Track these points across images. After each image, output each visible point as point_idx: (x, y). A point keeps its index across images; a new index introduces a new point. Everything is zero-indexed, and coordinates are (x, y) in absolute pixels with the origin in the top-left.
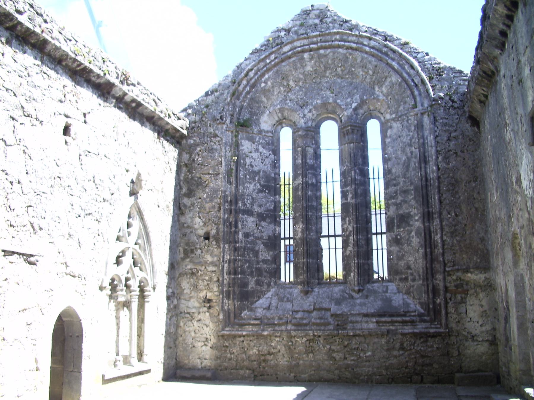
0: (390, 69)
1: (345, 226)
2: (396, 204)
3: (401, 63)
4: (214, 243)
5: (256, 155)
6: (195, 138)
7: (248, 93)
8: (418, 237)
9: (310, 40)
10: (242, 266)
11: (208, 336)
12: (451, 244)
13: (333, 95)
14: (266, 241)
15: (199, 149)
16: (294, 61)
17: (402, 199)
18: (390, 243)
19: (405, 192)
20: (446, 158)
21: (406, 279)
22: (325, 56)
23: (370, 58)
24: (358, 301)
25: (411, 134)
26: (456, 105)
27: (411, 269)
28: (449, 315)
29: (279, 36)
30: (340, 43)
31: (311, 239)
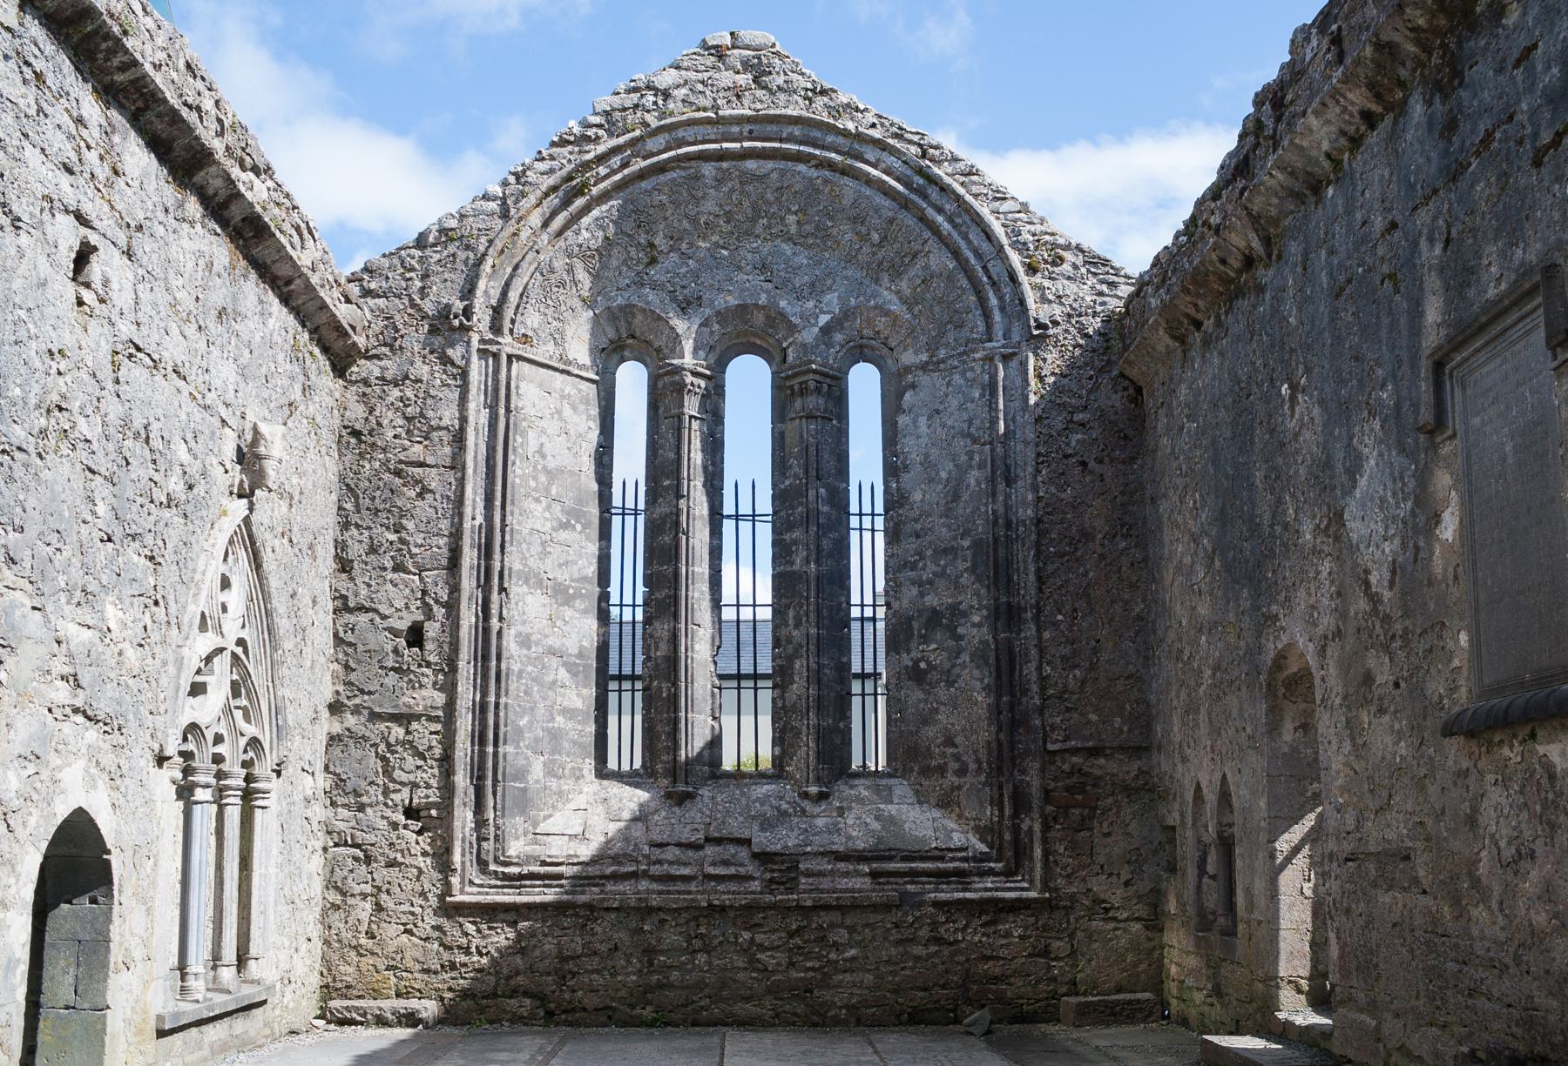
0: (927, 234)
3: (959, 220)
13: (770, 285)
16: (674, 180)
17: (938, 569)
19: (950, 551)
22: (761, 178)
23: (879, 199)
24: (820, 822)
27: (955, 746)
30: (802, 148)
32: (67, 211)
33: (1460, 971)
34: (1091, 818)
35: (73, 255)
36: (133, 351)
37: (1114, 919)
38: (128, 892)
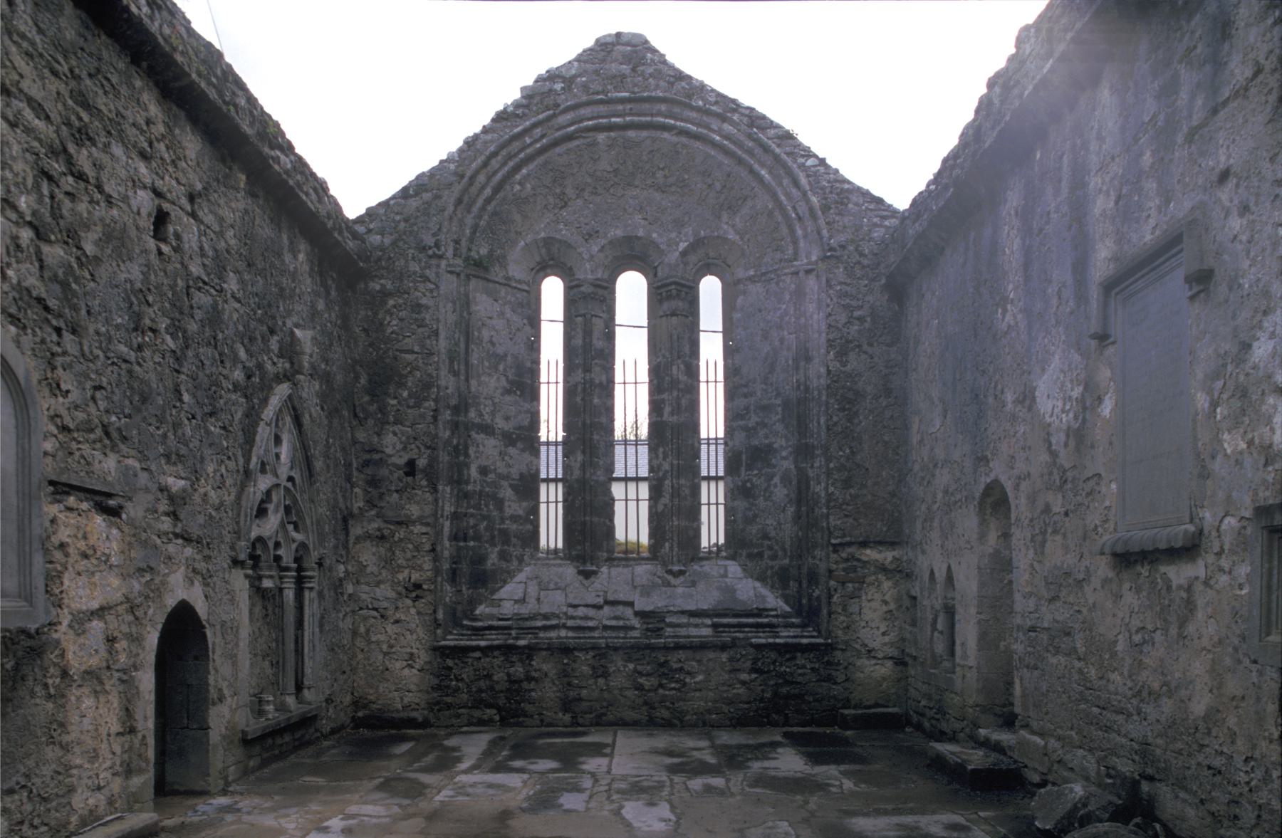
1: (655, 463)
2: (746, 429)
4: (424, 483)
5: (499, 323)
6: (383, 281)
7: (488, 201)
8: (785, 487)
9: (612, 107)
10: (475, 526)
11: (415, 651)
12: (840, 500)
14: (515, 482)
15: (391, 302)
16: (578, 146)
17: (759, 420)
18: (732, 494)
19: (766, 408)
20: (842, 354)
21: (760, 555)
23: (721, 157)
24: (680, 590)
25: (784, 306)
26: (866, 262)
28: (833, 616)
29: (550, 90)
31: (597, 481)
32: (145, 187)
33: (1101, 714)
34: (860, 589)
35: (152, 220)
36: (201, 285)
37: (875, 657)
38: (218, 652)
